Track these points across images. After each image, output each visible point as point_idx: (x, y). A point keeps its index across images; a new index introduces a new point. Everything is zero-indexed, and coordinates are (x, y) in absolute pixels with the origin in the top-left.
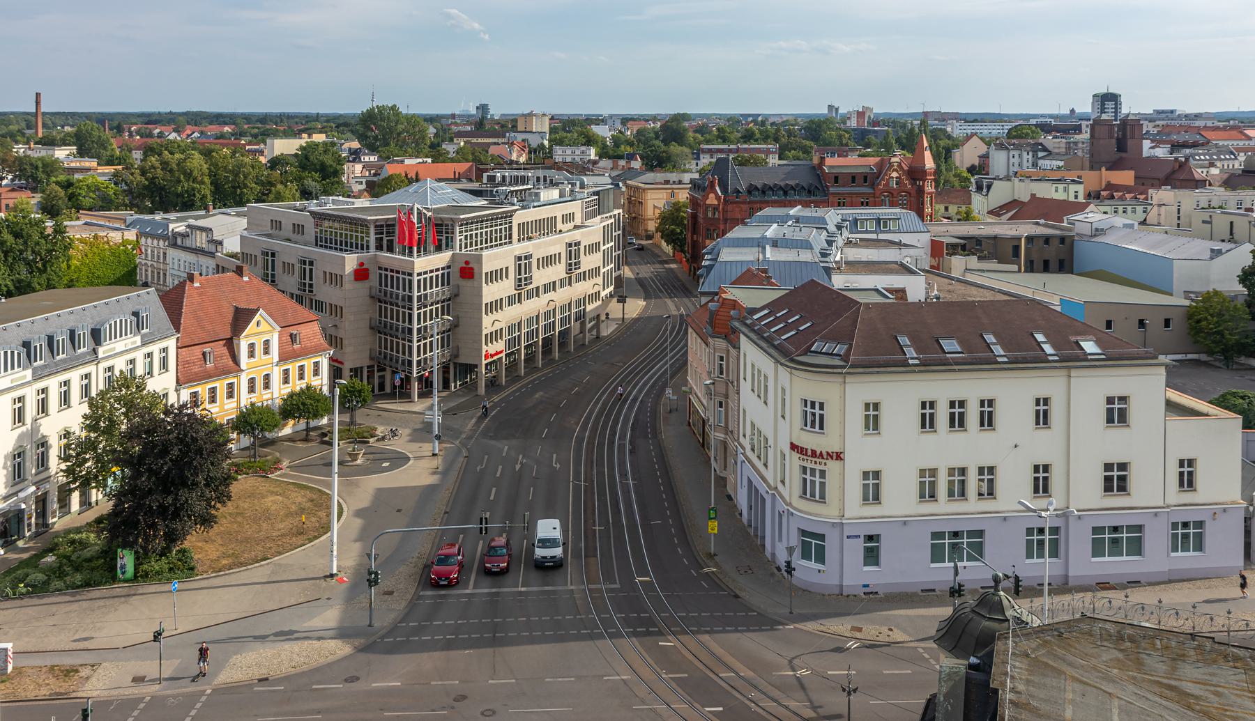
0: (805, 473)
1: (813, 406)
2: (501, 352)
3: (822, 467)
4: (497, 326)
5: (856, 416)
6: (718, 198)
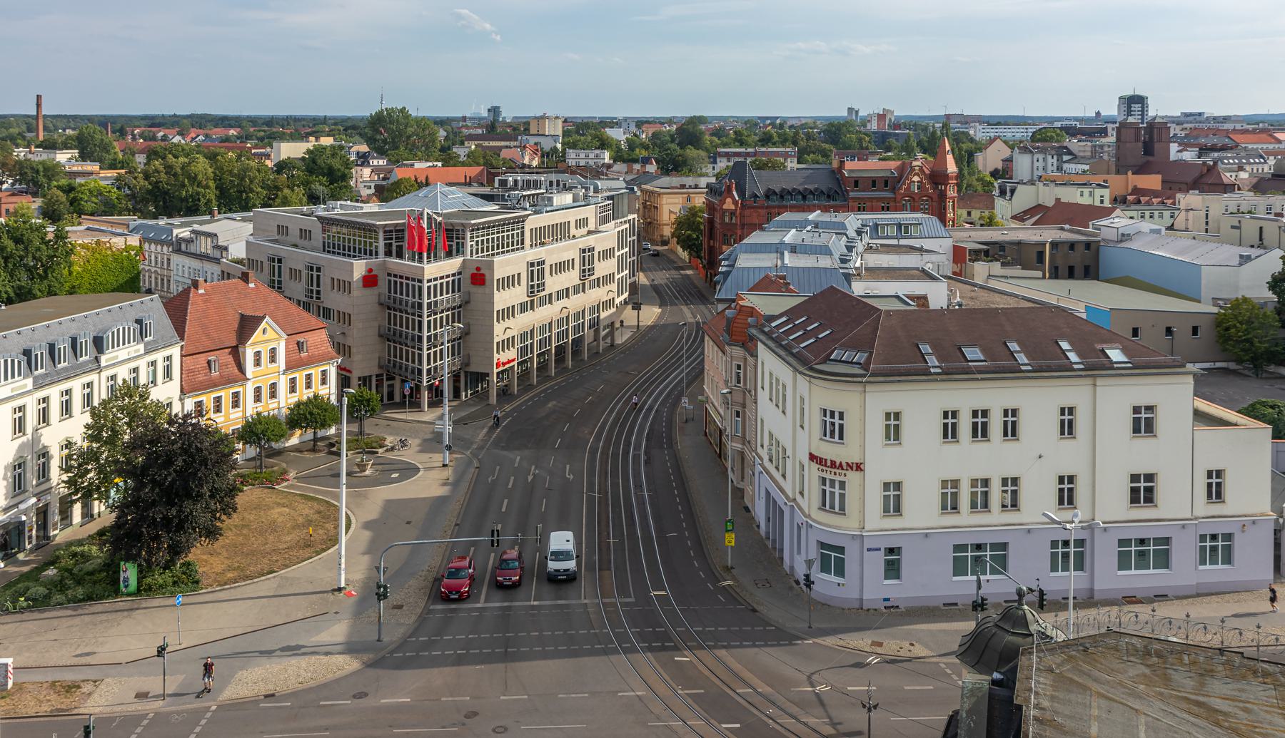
0: (824, 484)
1: (832, 415)
2: (513, 360)
3: (842, 478)
4: (509, 334)
5: (876, 426)
6: (735, 202)
